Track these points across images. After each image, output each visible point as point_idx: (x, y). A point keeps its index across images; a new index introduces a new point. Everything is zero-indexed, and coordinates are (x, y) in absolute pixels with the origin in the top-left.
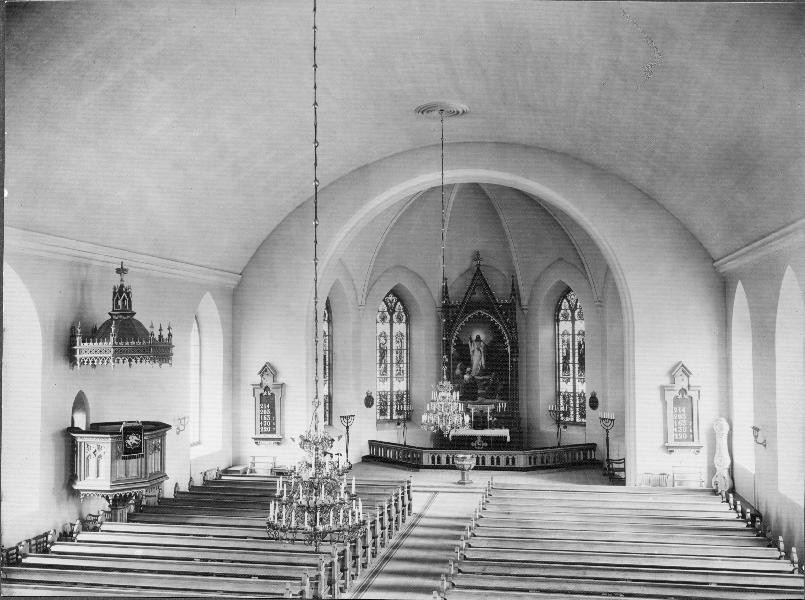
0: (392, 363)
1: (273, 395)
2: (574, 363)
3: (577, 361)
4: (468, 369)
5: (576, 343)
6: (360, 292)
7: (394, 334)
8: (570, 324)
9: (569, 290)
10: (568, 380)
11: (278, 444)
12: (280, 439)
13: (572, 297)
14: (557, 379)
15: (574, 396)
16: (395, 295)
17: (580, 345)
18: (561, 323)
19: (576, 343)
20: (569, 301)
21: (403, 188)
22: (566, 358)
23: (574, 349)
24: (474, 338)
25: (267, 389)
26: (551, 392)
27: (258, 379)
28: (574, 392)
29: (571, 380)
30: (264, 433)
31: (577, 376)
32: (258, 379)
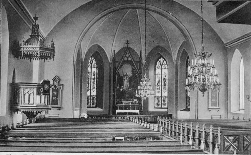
0: (91, 84)
6: (146, 56)
8: (160, 70)
11: (60, 109)
12: (60, 107)
15: (90, 96)
20: (160, 62)
21: (233, 11)
28: (90, 95)
29: (160, 92)
31: (163, 89)
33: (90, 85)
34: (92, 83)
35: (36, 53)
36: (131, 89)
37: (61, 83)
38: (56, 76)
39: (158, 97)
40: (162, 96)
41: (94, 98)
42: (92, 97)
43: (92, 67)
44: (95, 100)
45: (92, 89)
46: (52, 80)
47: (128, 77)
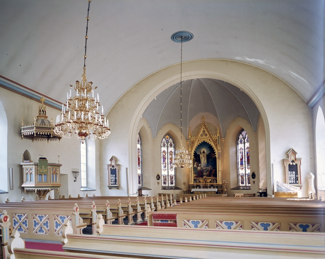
0: (168, 164)
1: (115, 169)
2: (245, 162)
3: (246, 160)
4: (200, 165)
5: (246, 153)
7: (169, 152)
9: (243, 130)
10: (243, 169)
11: (118, 189)
12: (118, 187)
13: (244, 133)
14: (237, 169)
16: (169, 136)
17: (247, 154)
18: (239, 145)
19: (246, 153)
20: (242, 135)
22: (242, 159)
23: (245, 155)
24: (202, 152)
25: (113, 166)
26: (235, 175)
27: (109, 163)
28: (168, 175)
30: (112, 184)
31: (246, 166)
32: (109, 163)
33: (167, 164)
34: (169, 163)
35: (32, 132)
36: (209, 167)
37: (119, 163)
38: (112, 157)
39: (242, 175)
40: (246, 173)
41: (173, 177)
42: (171, 176)
43: (168, 147)
44: (174, 180)
45: (169, 168)
46: (110, 160)
47: (205, 154)
